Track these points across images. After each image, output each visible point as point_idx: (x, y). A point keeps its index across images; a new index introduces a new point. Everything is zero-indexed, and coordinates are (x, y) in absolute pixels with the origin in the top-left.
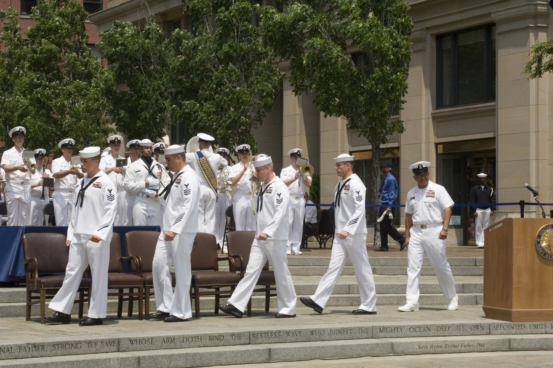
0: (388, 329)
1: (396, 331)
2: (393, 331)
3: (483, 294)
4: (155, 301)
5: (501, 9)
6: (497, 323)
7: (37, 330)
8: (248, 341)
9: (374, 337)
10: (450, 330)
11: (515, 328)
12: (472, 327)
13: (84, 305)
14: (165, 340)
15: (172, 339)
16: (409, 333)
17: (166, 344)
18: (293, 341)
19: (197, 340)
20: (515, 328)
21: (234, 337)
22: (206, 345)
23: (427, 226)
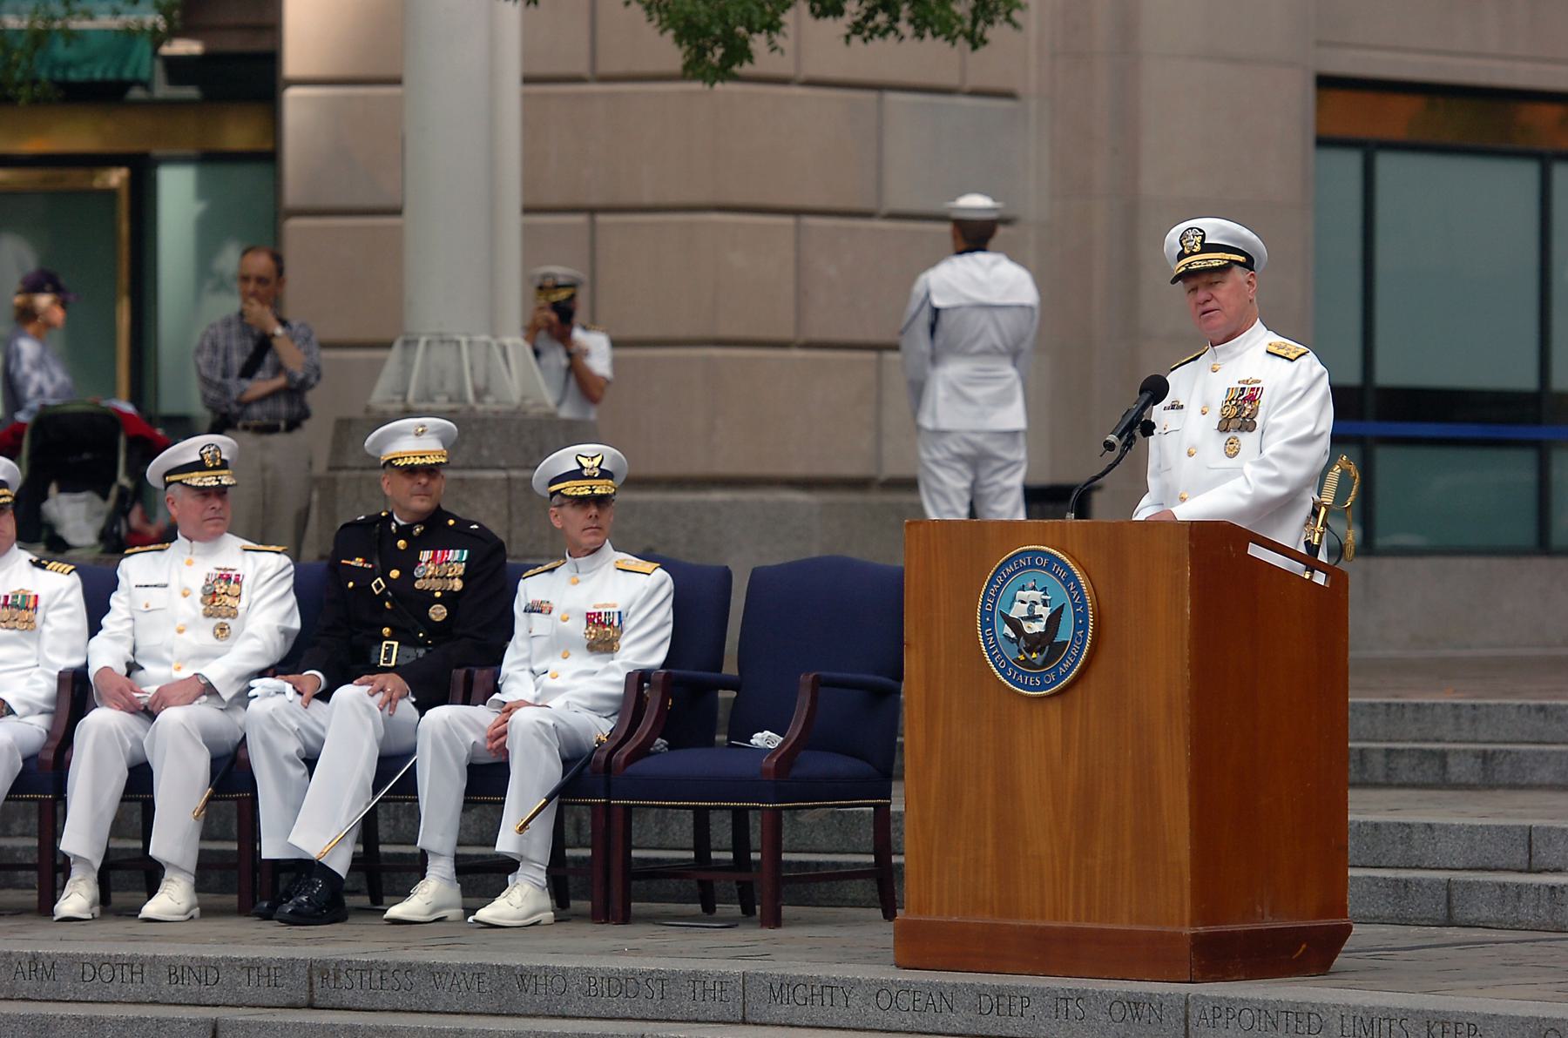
0: (800, 991)
1: (827, 1000)
2: (818, 999)
3: (34, 842)
4: (903, 865)
5: (1183, 361)
6: (1213, 999)
7: (312, 930)
8: (303, 996)
9: (749, 1018)
10: (1028, 1012)
11: (1282, 1025)
12: (1117, 1008)
13: (1352, 889)
14: (776, 987)
15: (48, 964)
16: (167, 989)
17: (27, 983)
18: (457, 1008)
19: (128, 976)
20: (1282, 1025)
21: (254, 974)
22: (159, 998)
23: (560, 674)
